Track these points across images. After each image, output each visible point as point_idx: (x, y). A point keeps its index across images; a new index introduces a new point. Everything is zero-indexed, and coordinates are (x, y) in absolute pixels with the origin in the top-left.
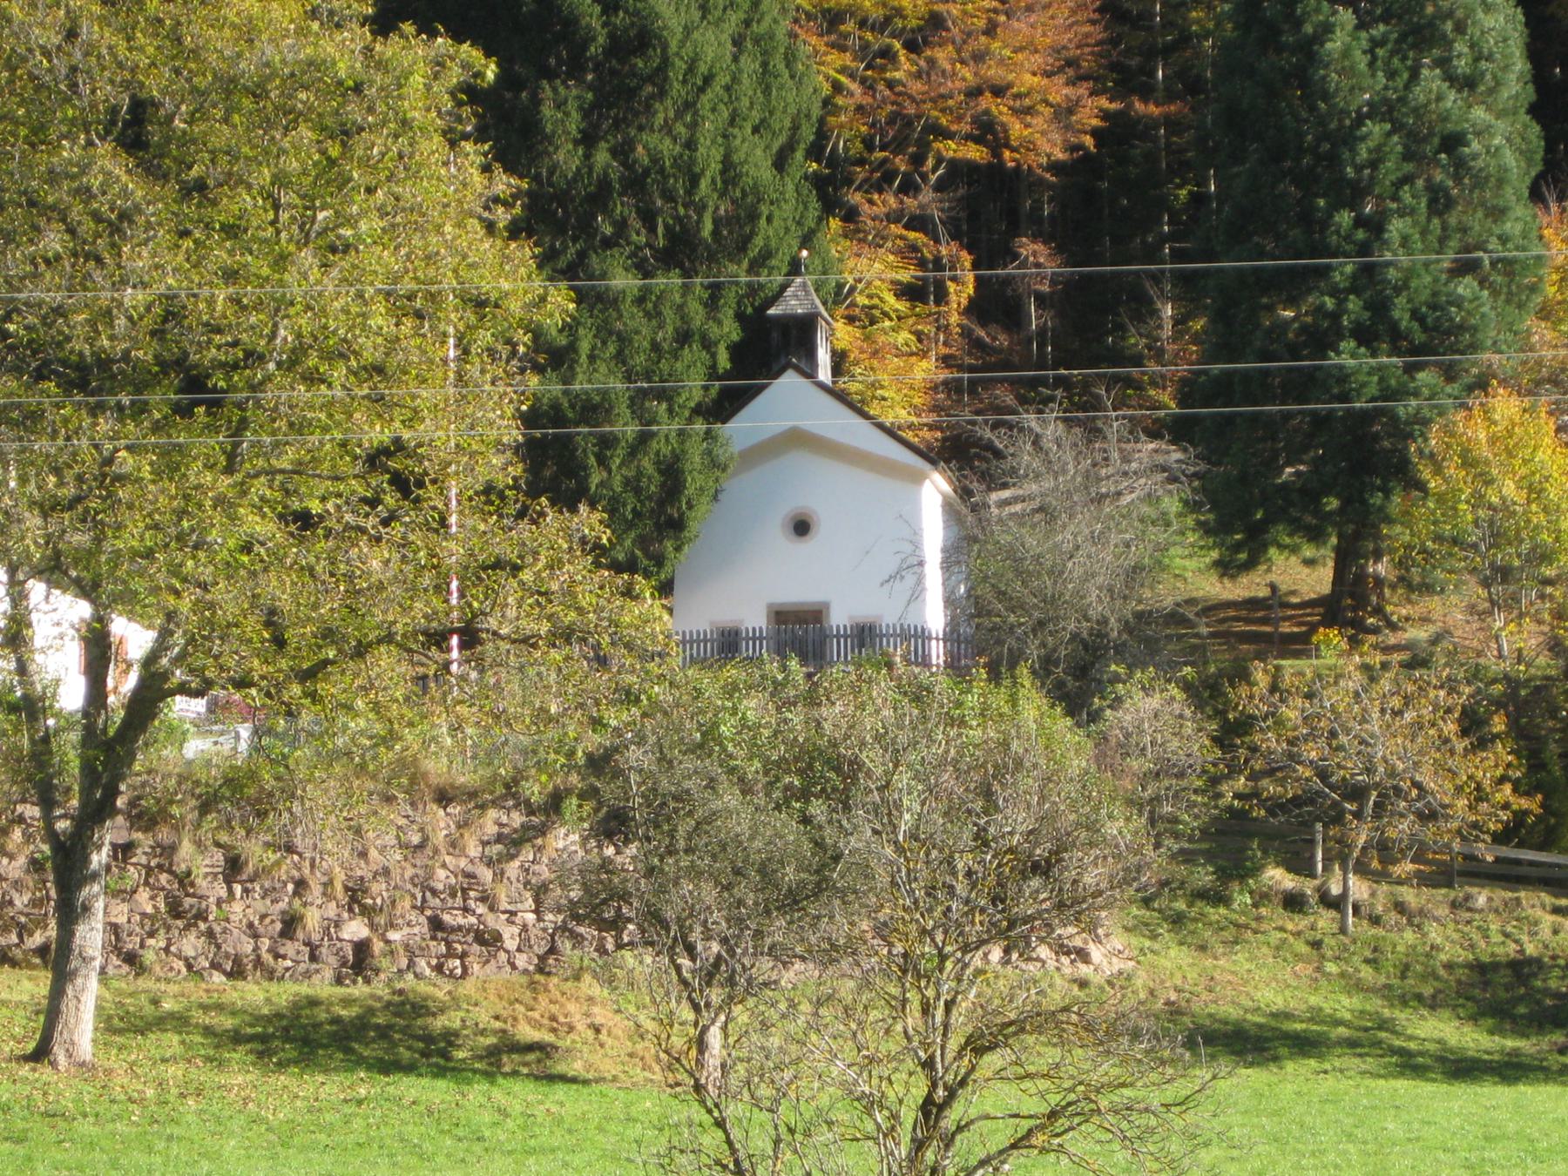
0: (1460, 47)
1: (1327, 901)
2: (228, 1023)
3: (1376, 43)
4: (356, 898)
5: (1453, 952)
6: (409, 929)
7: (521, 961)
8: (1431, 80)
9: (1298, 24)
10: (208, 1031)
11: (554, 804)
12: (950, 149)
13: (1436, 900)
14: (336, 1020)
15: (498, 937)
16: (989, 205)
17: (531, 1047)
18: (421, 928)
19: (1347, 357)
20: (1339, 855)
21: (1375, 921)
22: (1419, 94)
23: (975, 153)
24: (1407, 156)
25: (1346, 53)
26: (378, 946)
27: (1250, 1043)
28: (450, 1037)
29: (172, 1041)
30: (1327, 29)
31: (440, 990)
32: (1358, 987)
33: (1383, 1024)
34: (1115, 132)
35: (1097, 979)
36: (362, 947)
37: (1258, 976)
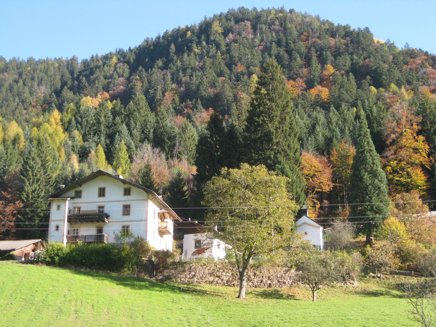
0: (379, 177)
1: (378, 277)
2: (257, 293)
3: (370, 177)
4: (269, 278)
5: (393, 283)
6: (275, 282)
7: (288, 285)
8: (376, 181)
9: (360, 174)
10: (255, 294)
11: (291, 267)
12: (316, 189)
13: (390, 276)
14: (269, 293)
15: (286, 283)
16: (321, 196)
17: (292, 296)
18: (277, 282)
19: (369, 213)
20: (379, 271)
21: (384, 279)
22: (375, 182)
23: (320, 190)
24: (374, 190)
25: (367, 178)
26: (272, 284)
27: (375, 294)
28: (282, 295)
29: (251, 295)
30: (364, 175)
31: (280, 289)
32: (384, 287)
33: (389, 292)
34: (334, 187)
35: (355, 287)
36: (270, 284)
37: (373, 287)
